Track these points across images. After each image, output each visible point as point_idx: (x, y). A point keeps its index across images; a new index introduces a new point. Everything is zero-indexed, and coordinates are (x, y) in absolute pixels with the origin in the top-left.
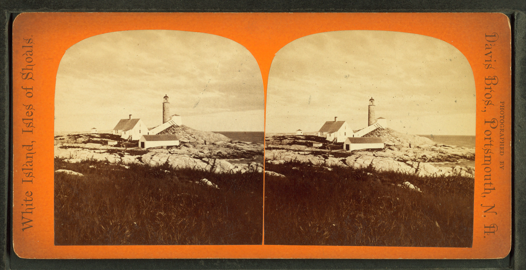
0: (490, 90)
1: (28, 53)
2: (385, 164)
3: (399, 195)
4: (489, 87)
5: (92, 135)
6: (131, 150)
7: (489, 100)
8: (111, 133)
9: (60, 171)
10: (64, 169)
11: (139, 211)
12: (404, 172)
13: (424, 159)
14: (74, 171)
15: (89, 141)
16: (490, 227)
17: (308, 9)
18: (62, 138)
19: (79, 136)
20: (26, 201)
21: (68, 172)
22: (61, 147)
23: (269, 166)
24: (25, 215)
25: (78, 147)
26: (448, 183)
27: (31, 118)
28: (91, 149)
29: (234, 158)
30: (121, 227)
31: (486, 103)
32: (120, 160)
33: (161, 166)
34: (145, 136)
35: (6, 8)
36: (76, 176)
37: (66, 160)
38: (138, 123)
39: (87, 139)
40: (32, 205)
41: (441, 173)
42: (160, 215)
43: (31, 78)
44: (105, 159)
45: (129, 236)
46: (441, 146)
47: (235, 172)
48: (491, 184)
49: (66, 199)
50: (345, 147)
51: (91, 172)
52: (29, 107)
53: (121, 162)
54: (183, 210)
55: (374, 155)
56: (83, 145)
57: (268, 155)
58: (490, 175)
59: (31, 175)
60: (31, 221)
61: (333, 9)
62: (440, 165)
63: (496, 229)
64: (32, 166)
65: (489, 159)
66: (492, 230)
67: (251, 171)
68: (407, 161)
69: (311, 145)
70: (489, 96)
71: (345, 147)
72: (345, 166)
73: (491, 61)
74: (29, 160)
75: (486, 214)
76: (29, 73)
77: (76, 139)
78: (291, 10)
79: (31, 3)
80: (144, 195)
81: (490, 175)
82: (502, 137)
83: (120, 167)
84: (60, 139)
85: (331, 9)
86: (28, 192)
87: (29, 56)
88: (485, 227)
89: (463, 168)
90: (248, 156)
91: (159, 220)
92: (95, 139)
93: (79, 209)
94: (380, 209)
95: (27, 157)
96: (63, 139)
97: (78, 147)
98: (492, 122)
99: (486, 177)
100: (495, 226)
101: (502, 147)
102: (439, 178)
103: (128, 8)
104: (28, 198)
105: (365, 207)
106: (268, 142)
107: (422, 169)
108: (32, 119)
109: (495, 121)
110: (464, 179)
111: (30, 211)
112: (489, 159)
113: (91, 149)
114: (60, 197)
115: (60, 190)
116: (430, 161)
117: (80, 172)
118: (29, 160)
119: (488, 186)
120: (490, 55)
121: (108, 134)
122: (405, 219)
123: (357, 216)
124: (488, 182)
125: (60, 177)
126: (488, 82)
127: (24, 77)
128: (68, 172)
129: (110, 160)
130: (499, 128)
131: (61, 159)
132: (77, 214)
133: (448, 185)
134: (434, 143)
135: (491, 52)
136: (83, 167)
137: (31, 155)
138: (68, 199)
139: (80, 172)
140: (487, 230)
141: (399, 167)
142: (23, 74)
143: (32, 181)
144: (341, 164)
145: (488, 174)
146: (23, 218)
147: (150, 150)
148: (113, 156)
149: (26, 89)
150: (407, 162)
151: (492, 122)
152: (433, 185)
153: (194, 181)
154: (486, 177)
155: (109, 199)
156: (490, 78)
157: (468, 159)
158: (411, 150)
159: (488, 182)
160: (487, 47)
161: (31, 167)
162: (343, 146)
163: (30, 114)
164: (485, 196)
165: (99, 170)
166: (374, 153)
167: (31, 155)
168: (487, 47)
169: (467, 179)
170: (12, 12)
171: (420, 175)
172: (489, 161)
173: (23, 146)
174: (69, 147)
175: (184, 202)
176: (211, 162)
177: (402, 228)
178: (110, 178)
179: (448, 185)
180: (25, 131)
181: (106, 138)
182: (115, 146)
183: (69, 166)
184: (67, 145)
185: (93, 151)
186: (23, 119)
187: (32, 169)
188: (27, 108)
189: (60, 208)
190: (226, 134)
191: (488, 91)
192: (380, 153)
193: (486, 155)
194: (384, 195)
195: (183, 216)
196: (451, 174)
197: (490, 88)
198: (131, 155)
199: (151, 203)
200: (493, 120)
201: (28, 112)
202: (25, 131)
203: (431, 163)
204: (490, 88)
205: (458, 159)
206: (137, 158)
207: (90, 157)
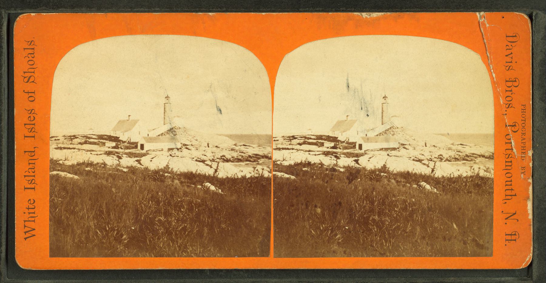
1: (29, 56)
2: (399, 164)
3: (414, 196)
4: (510, 89)
5: (89, 136)
6: (130, 153)
7: (509, 103)
8: (109, 134)
9: (55, 173)
10: (59, 170)
11: (138, 216)
12: (420, 172)
13: (440, 158)
14: (69, 173)
15: (86, 143)
16: (511, 235)
17: (317, 9)
18: (57, 138)
19: (75, 137)
20: (28, 209)
21: (63, 174)
22: (56, 148)
23: (277, 167)
24: (27, 224)
25: (74, 148)
27: (33, 123)
28: (88, 151)
29: (238, 162)
31: (507, 106)
32: (118, 162)
33: (161, 169)
34: (145, 138)
35: (4, 8)
37: (61, 162)
38: (137, 124)
39: (83, 141)
40: (34, 213)
41: (459, 173)
42: (160, 220)
43: (33, 82)
44: (102, 162)
45: (126, 241)
46: (458, 145)
47: (240, 177)
48: (512, 189)
49: (60, 202)
50: (357, 147)
51: (87, 175)
52: (31, 111)
53: (119, 165)
54: (184, 216)
55: (388, 155)
56: (79, 146)
57: (277, 156)
58: (511, 181)
59: (33, 182)
60: (34, 229)
61: (344, 9)
62: (457, 165)
63: (517, 237)
64: (34, 172)
66: (513, 237)
67: (256, 175)
68: (423, 160)
69: (322, 145)
71: (357, 147)
72: (358, 166)
73: (511, 62)
75: (507, 221)
76: (30, 77)
77: (72, 140)
78: (300, 10)
79: (29, 2)
80: (143, 199)
83: (118, 170)
84: (55, 140)
85: (341, 9)
86: (30, 200)
87: (31, 59)
88: (506, 235)
89: (482, 167)
90: (255, 159)
92: (92, 140)
93: (73, 212)
94: (395, 211)
95: (29, 164)
96: (278, 140)
98: (513, 126)
99: (507, 183)
100: (517, 233)
101: (524, 151)
102: (456, 178)
103: (130, 8)
104: (31, 206)
105: (379, 209)
107: (439, 168)
108: (34, 124)
109: (517, 124)
110: (482, 178)
111: (33, 219)
112: (510, 164)
113: (88, 151)
114: (54, 200)
115: (53, 192)
116: (447, 160)
117: (76, 174)
119: (509, 193)
120: (510, 56)
121: (106, 135)
122: (421, 220)
123: (371, 219)
124: (510, 187)
126: (510, 84)
127: (26, 80)
128: (63, 174)
129: (107, 162)
130: (520, 132)
131: (56, 161)
132: (72, 217)
133: (466, 185)
134: (451, 142)
135: (512, 53)
136: (78, 169)
137: (33, 162)
138: (62, 202)
139: (76, 174)
140: (509, 237)
141: (415, 167)
142: (25, 77)
143: (34, 188)
145: (509, 179)
146: (25, 226)
147: (149, 152)
149: (28, 93)
150: (423, 162)
151: (513, 126)
152: (450, 185)
153: (196, 185)
154: (507, 183)
155: (106, 204)
156: (511, 80)
157: (486, 158)
158: (427, 149)
159: (510, 187)
161: (33, 174)
162: (355, 146)
163: (32, 118)
164: (506, 203)
166: (388, 152)
167: (33, 162)
171: (436, 176)
173: (25, 152)
175: (185, 207)
176: (214, 165)
177: (418, 229)
178: (107, 181)
180: (27, 137)
181: (103, 139)
182: (113, 148)
183: (63, 168)
184: (62, 146)
185: (89, 152)
186: (25, 124)
187: (34, 176)
188: (29, 112)
189: (54, 211)
190: (230, 136)
191: (509, 94)
192: (393, 153)
195: (184, 221)
196: (469, 174)
197: (511, 91)
198: (130, 157)
199: (150, 207)
200: (514, 124)
201: (30, 117)
202: (27, 137)
203: (447, 162)
204: (511, 91)
205: (476, 158)
207: (86, 160)
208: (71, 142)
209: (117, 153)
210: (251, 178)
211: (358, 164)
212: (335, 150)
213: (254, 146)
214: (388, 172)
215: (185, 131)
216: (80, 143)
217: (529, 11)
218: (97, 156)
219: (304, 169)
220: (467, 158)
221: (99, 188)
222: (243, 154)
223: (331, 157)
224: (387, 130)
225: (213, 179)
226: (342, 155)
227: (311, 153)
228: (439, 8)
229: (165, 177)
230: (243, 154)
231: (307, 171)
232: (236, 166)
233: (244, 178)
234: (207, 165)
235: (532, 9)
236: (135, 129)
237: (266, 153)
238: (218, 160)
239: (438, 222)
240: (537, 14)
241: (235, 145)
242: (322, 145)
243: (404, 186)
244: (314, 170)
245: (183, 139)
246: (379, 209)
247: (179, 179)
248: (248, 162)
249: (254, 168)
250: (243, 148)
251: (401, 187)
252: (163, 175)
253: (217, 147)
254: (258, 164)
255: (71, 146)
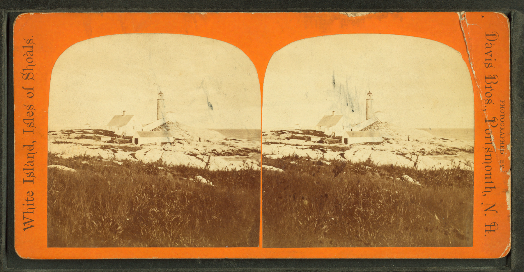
0: (490, 89)
3: (397, 188)
4: (489, 86)
5: (85, 131)
6: (125, 147)
7: (489, 98)
8: (105, 129)
9: (53, 166)
10: (56, 164)
11: (132, 208)
12: (403, 165)
13: (423, 152)
14: (66, 166)
15: (82, 137)
16: (490, 226)
17: (305, 9)
18: (54, 133)
19: (72, 132)
20: (27, 201)
21: (60, 167)
22: (53, 143)
23: (266, 160)
25: (71, 143)
26: (447, 175)
27: (31, 118)
28: (84, 145)
30: (114, 223)
31: (487, 102)
32: (113, 156)
33: (155, 163)
34: (139, 133)
35: (3, 8)
36: (69, 172)
37: (58, 156)
38: (132, 120)
39: (80, 135)
40: (33, 205)
41: (440, 166)
42: (153, 212)
43: (32, 79)
44: (98, 155)
45: (121, 232)
46: (231, 140)
48: (491, 182)
49: (57, 194)
50: (343, 141)
51: (83, 168)
53: (114, 159)
54: (177, 207)
55: (372, 149)
56: (76, 141)
57: (266, 150)
60: (33, 221)
61: (330, 8)
62: (439, 159)
63: (496, 227)
64: (32, 166)
65: (489, 157)
66: (493, 228)
68: (406, 154)
69: (309, 139)
70: (490, 95)
71: (343, 141)
72: (344, 159)
73: (491, 60)
74: (30, 160)
76: (29, 74)
77: (69, 135)
79: (28, 2)
80: (137, 192)
81: (491, 174)
82: (502, 136)
83: (113, 163)
84: (53, 134)
85: (327, 8)
86: (29, 192)
87: (29, 56)
88: (486, 226)
89: (462, 161)
90: (244, 152)
91: (152, 217)
93: (70, 204)
94: (379, 203)
96: (56, 134)
97: (71, 143)
98: (492, 121)
99: (487, 176)
100: (496, 224)
101: (503, 145)
102: (438, 171)
103: (125, 8)
104: (30, 198)
105: (364, 201)
106: (265, 137)
107: (421, 162)
108: (33, 119)
109: (496, 119)
110: (463, 171)
111: (32, 211)
112: (489, 157)
113: (84, 145)
114: (52, 192)
115: (51, 185)
116: (429, 154)
117: (73, 167)
118: (30, 160)
119: (488, 185)
120: (490, 54)
121: (102, 130)
122: (404, 212)
123: (356, 210)
124: (489, 180)
125: (52, 173)
126: (489, 81)
127: (25, 77)
128: (60, 167)
129: (102, 156)
130: (499, 127)
131: (54, 155)
132: (69, 209)
133: (447, 178)
135: (491, 51)
136: (75, 162)
137: (32, 155)
138: (59, 194)
139: (73, 167)
140: (489, 228)
141: (398, 161)
142: (24, 74)
143: (33, 181)
144: (339, 158)
145: (489, 172)
146: (24, 218)
147: (143, 146)
148: (106, 152)
149: (27, 89)
150: (406, 156)
151: (492, 121)
152: (432, 178)
153: (188, 178)
154: (487, 176)
155: (102, 196)
156: (490, 77)
157: (467, 152)
158: (410, 144)
159: (489, 180)
160: (487, 46)
161: (31, 167)
162: (341, 140)
163: (31, 114)
164: (485, 195)
165: (92, 166)
166: (372, 146)
167: (32, 155)
168: (487, 46)
169: (466, 172)
170: (9, 11)
171: (419, 169)
172: (490, 159)
173: (24, 146)
174: (62, 142)
175: (178, 199)
178: (103, 173)
179: (447, 178)
181: (99, 133)
182: (109, 142)
183: (61, 161)
184: (60, 140)
185: (86, 146)
186: (24, 120)
187: (33, 169)
188: (28, 108)
191: (488, 90)
192: (378, 147)
193: (487, 154)
194: (382, 188)
195: (176, 213)
196: (451, 167)
197: (490, 87)
198: (124, 151)
199: (144, 199)
200: (493, 119)
201: (29, 112)
203: (429, 156)
204: (490, 87)
205: (457, 152)
206: (131, 155)
207: (83, 153)
208: (68, 136)
209: (112, 147)
210: (241, 171)
211: (344, 157)
212: (321, 144)
213: (243, 140)
214: (372, 165)
215: (178, 126)
216: (77, 138)
217: (507, 11)
218: (93, 150)
219: (292, 162)
220: (448, 152)
221: (95, 180)
222: (233, 148)
223: (318, 151)
224: (372, 125)
225: (204, 173)
226: (328, 149)
227: (298, 147)
228: (421, 8)
229: (158, 170)
230: (233, 148)
231: (294, 165)
232: (226, 159)
233: (234, 171)
234: (199, 158)
235: (510, 8)
236: (130, 124)
237: (255, 147)
238: (209, 154)
239: (421, 213)
240: (515, 14)
241: (226, 139)
242: (309, 139)
243: (388, 179)
244: (301, 163)
245: (175, 133)
246: (364, 201)
247: (172, 172)
248: (238, 156)
249: (244, 161)
250: (233, 143)
251: (385, 179)
252: (156, 168)
253: (208, 141)
254: (248, 157)
255: (68, 141)
